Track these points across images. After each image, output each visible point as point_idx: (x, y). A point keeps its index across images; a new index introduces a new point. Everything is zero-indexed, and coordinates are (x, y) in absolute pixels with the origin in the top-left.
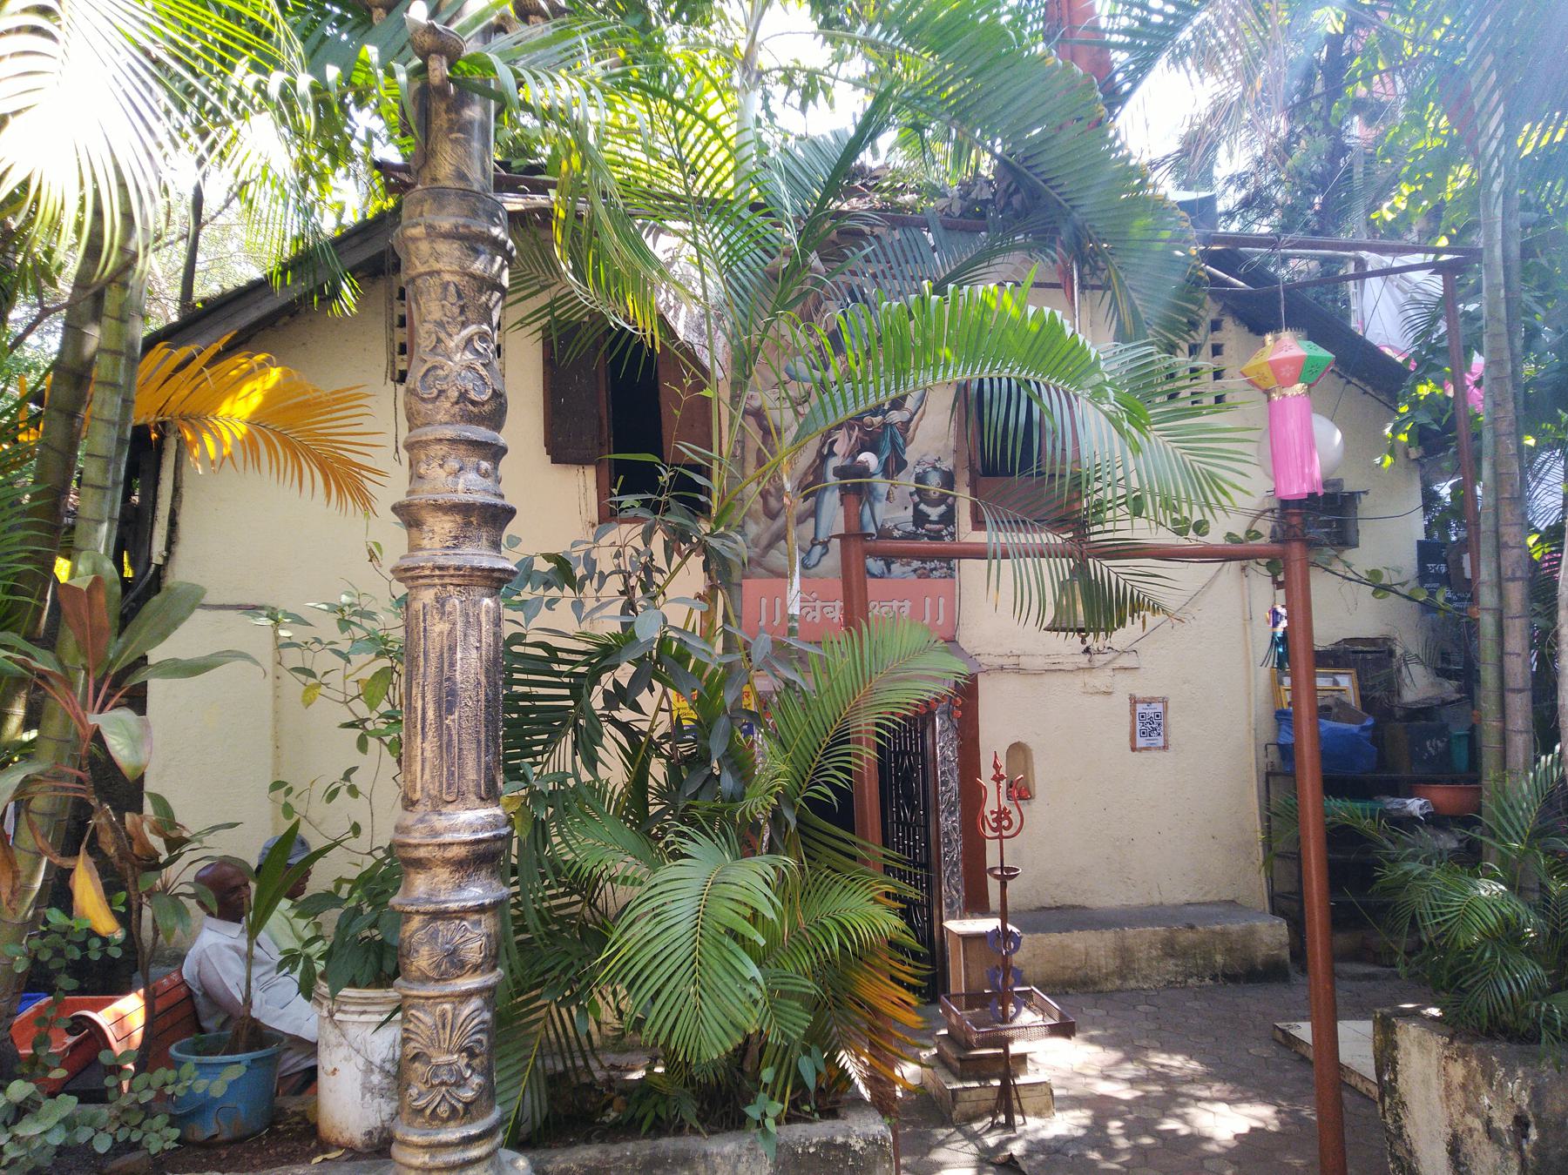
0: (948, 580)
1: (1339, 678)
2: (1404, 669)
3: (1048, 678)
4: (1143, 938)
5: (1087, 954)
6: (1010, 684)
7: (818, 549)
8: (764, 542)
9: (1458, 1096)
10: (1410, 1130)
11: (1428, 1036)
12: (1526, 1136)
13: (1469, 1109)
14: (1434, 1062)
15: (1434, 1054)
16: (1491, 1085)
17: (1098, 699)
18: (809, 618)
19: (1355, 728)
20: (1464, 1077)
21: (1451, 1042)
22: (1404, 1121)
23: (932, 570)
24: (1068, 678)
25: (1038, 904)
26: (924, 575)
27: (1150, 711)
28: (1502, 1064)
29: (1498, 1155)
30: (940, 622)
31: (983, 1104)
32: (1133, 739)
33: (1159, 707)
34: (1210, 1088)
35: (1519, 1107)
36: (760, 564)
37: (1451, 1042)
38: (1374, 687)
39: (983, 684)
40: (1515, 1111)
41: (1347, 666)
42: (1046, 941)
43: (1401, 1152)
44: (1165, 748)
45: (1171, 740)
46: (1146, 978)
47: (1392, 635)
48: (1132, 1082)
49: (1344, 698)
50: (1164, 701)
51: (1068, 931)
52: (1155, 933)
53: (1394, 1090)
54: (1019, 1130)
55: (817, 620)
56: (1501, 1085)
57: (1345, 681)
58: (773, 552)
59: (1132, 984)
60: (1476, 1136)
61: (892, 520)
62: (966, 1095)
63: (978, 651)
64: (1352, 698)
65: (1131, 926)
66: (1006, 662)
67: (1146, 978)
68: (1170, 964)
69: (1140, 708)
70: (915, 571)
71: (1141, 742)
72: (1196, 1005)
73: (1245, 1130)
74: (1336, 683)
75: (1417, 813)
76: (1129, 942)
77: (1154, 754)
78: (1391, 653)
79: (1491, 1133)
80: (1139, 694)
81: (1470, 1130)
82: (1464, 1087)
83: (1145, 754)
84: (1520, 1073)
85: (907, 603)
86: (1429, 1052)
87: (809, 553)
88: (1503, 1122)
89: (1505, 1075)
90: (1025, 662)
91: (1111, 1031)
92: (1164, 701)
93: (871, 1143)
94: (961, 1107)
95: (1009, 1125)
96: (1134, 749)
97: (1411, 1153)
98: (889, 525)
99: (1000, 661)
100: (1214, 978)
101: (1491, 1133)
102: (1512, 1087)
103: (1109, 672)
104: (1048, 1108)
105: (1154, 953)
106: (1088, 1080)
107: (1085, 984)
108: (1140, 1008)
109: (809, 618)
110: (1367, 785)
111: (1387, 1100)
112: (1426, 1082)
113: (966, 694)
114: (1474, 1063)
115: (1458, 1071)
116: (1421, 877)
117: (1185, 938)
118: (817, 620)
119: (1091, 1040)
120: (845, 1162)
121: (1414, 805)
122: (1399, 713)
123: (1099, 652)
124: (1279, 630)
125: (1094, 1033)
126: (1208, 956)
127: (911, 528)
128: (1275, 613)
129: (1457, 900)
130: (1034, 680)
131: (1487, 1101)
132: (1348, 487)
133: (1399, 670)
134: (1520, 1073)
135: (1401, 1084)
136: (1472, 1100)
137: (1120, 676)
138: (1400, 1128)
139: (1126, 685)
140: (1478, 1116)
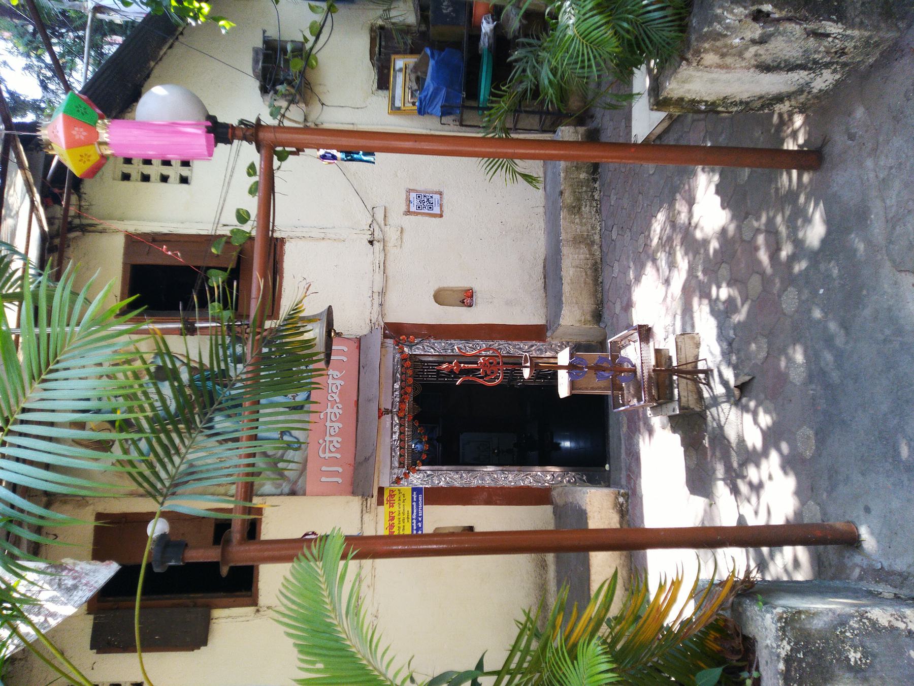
1: (397, 67)
2: (393, 21)
4: (568, 227)
5: (577, 267)
6: (393, 299)
9: (729, 60)
10: (745, 97)
11: (679, 76)
12: (768, 14)
13: (740, 54)
14: (700, 74)
15: (693, 73)
16: (726, 36)
17: (405, 236)
18: (338, 446)
19: (432, 63)
20: (716, 54)
21: (687, 60)
22: (737, 99)
24: (390, 258)
27: (416, 202)
28: (710, 24)
29: (780, 38)
30: (346, 349)
31: (690, 387)
32: (435, 216)
33: (413, 195)
34: (679, 213)
35: (746, 16)
36: (295, 482)
37: (687, 60)
38: (405, 43)
39: (394, 317)
40: (749, 20)
41: (389, 61)
43: (758, 104)
44: (441, 194)
45: (436, 189)
46: (593, 228)
47: (368, 25)
49: (411, 66)
50: (409, 191)
52: (565, 219)
53: (713, 103)
54: (711, 365)
55: (340, 440)
56: (728, 28)
57: (400, 63)
59: (597, 237)
60: (761, 52)
62: (683, 400)
64: (412, 60)
66: (376, 302)
67: (593, 228)
68: (585, 210)
69: (413, 209)
71: (436, 210)
72: (613, 198)
73: (717, 200)
74: (400, 70)
75: (491, 26)
76: (569, 237)
77: (445, 202)
78: (382, 28)
79: (762, 41)
80: (404, 208)
81: (756, 55)
82: (723, 55)
83: (445, 209)
84: (719, 11)
86: (691, 76)
88: (756, 30)
89: (719, 23)
90: (377, 288)
91: (631, 264)
92: (409, 191)
93: (784, 631)
94: (692, 404)
95: (708, 372)
96: (441, 216)
97: (761, 98)
99: (376, 306)
100: (595, 180)
101: (762, 41)
102: (730, 19)
104: (693, 338)
105: (577, 220)
106: (669, 295)
107: (596, 270)
109: (338, 446)
110: (473, 70)
111: (720, 109)
112: (713, 81)
113: (396, 332)
114: (706, 45)
115: (710, 58)
116: (554, 71)
117: (568, 198)
118: (340, 440)
119: (638, 279)
120: (800, 661)
121: (487, 27)
122: (423, 28)
123: (372, 234)
124: (339, 155)
126: (580, 184)
128: (323, 157)
129: (577, 45)
130: (390, 282)
131: (737, 40)
132: (259, 44)
133: (393, 24)
134: (719, 11)
135: (710, 99)
136: (733, 51)
137: (390, 221)
138: (741, 102)
139: (397, 217)
140: (747, 49)
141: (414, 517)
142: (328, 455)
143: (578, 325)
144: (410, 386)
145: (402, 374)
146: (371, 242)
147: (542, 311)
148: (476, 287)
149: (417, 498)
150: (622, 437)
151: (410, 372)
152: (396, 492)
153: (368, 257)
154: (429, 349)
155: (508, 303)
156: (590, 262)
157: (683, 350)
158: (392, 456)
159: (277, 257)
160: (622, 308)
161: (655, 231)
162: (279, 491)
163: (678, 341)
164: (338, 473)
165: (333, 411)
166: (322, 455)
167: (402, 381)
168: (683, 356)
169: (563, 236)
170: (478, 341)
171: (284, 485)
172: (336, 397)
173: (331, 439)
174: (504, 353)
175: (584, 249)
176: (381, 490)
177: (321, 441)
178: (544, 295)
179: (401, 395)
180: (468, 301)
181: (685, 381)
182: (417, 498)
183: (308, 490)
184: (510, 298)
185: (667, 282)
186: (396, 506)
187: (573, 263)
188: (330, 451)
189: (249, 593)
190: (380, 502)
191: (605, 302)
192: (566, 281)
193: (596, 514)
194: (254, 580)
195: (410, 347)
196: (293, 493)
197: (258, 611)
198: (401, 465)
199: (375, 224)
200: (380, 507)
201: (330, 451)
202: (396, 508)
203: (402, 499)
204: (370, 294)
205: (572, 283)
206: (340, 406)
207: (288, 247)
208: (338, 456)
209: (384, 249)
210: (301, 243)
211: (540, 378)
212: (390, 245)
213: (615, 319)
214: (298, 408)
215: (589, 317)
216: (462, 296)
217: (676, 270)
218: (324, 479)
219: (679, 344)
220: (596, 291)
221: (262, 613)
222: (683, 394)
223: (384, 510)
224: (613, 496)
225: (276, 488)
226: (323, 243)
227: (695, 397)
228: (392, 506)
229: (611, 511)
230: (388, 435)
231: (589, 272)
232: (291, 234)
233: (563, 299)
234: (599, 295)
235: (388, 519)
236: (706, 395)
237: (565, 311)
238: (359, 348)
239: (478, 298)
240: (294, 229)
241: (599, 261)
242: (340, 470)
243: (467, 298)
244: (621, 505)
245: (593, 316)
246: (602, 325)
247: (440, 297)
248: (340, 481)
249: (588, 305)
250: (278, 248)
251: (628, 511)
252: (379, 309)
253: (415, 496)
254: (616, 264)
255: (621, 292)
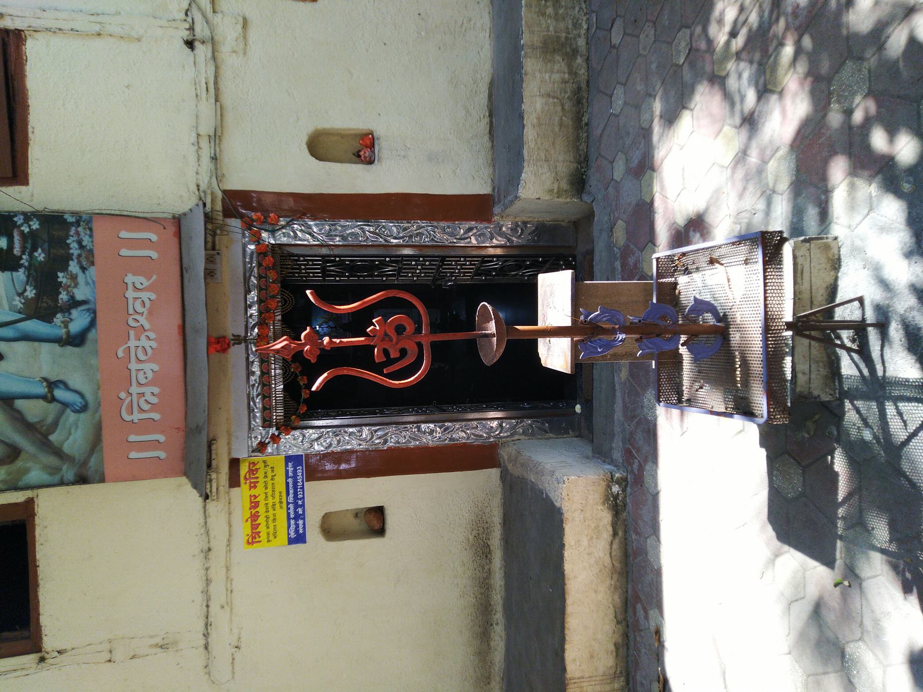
0: (95, 225)
3: (227, 98)
7: (59, 393)
8: (53, 461)
17: (252, 34)
23: (81, 247)
25: (487, 138)
26: (88, 258)
30: (154, 238)
31: (815, 352)
36: (85, 463)
39: (235, 183)
42: (532, 145)
46: (576, 25)
48: (767, 88)
51: (521, 117)
58: (66, 448)
59: (581, 42)
61: (10, 300)
62: (802, 379)
63: (193, 187)
65: (517, 36)
66: (206, 152)
67: (576, 25)
70: (84, 269)
76: (537, 40)
85: (130, 279)
87: (65, 405)
90: (206, 128)
98: (18, 302)
103: (217, 19)
104: (827, 247)
105: (550, 11)
107: (579, 102)
108: (616, 40)
109: (154, 400)
113: (241, 205)
118: (156, 390)
119: (670, 119)
123: (192, 29)
125: (658, 106)
127: (21, 275)
130: (229, 118)
141: (291, 499)
142: (136, 416)
143: (547, 197)
144: (274, 297)
145: (260, 277)
146: (190, 44)
147: (487, 172)
148: (380, 130)
149: (295, 472)
150: (617, 387)
151: (272, 275)
152: (260, 465)
153: (184, 73)
154: (306, 235)
155: (432, 158)
156: (569, 87)
157: (806, 275)
158: (250, 410)
159: (12, 67)
160: (628, 171)
161: (720, 22)
162: (56, 479)
163: (799, 254)
164: (159, 443)
165: (137, 343)
166: (127, 417)
167: (260, 289)
168: (805, 286)
169: (525, 39)
170: (383, 222)
171: (65, 468)
172: (143, 320)
173: (141, 390)
174: (426, 240)
175: (560, 64)
176: (235, 464)
177: (123, 395)
178: (489, 145)
179: (260, 312)
180: (366, 153)
181: (806, 341)
182: (295, 472)
183: (108, 473)
184: (429, 148)
185: (750, 122)
186: (260, 486)
187: (541, 90)
188: (141, 410)
189: (26, 633)
190: (234, 482)
191: (593, 157)
192: (530, 120)
193: (576, 514)
194: (32, 614)
195: (273, 232)
196: (82, 480)
197: (42, 659)
198: (267, 423)
199: (194, 10)
200: (235, 490)
201: (141, 410)
202: (259, 490)
203: (270, 474)
204: (193, 138)
205: (540, 125)
206: (152, 335)
207: (32, 48)
208: (156, 416)
209: (214, 58)
210: (56, 41)
211: (480, 275)
212: (225, 50)
213: (611, 190)
214: (77, 340)
215: (565, 185)
216: (356, 145)
217: (774, 98)
218: (133, 455)
219: (800, 261)
220: (578, 139)
221: (50, 661)
222: (802, 367)
223: (242, 493)
224: (604, 484)
225: (51, 474)
226: (98, 43)
227: (824, 372)
228: (253, 486)
229: (600, 507)
230: (243, 382)
231: (567, 106)
232: (36, 23)
233: (525, 152)
234: (583, 146)
235: (248, 505)
236: (848, 367)
237: (527, 175)
238: (179, 234)
239: (383, 148)
240: (40, 13)
241: (584, 86)
242: (162, 438)
243: (364, 149)
244: (616, 497)
245: (572, 183)
246: (586, 198)
247: (320, 146)
248: (162, 455)
249: (563, 163)
250: (12, 49)
251: (625, 505)
252: (212, 166)
253: (290, 469)
254: (619, 92)
255: (628, 142)
